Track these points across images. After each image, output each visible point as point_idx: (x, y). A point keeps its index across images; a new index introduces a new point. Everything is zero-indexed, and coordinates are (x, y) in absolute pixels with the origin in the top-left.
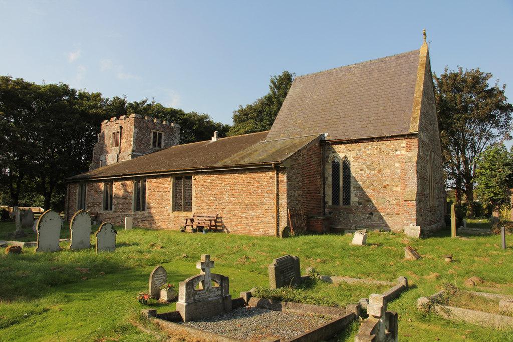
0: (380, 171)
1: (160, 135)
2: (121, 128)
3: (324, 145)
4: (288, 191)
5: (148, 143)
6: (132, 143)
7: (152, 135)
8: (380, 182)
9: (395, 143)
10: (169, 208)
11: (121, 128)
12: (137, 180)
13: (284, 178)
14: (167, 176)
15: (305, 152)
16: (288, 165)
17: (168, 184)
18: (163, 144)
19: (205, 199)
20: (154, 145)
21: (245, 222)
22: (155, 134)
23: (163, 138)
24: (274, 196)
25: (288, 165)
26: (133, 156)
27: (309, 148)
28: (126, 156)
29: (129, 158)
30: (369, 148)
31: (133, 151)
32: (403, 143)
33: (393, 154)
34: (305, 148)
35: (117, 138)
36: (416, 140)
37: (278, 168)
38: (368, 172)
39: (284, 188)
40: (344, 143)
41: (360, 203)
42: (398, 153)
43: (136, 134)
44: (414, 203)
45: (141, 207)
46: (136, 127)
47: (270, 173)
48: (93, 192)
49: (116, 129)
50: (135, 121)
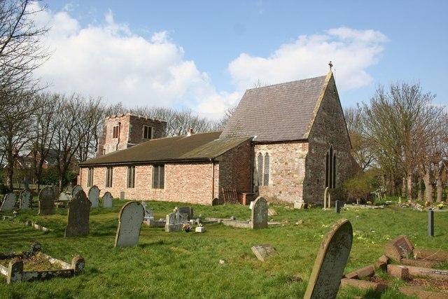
0: (286, 164)
1: (150, 129)
2: (120, 123)
3: (252, 144)
4: (220, 176)
5: (141, 135)
6: (128, 136)
7: (143, 129)
8: (286, 170)
9: (295, 145)
10: (150, 186)
11: (120, 123)
12: (156, 165)
13: (217, 167)
14: (103, 166)
15: (236, 150)
16: (221, 159)
17: (150, 169)
18: (152, 136)
19: (172, 180)
20: (145, 137)
21: (195, 195)
22: (146, 128)
23: (153, 131)
24: (211, 179)
25: (221, 159)
26: (128, 146)
27: (240, 147)
28: (124, 146)
29: (125, 147)
30: (280, 148)
31: (129, 142)
32: (301, 145)
33: (294, 152)
34: (236, 147)
35: (116, 132)
36: (308, 144)
37: (214, 162)
38: (279, 164)
39: (217, 174)
40: (266, 144)
41: (274, 185)
42: (297, 151)
43: (131, 129)
44: (302, 185)
45: (132, 185)
46: (131, 124)
47: (210, 165)
48: (99, 174)
49: (116, 125)
50: (130, 119)
